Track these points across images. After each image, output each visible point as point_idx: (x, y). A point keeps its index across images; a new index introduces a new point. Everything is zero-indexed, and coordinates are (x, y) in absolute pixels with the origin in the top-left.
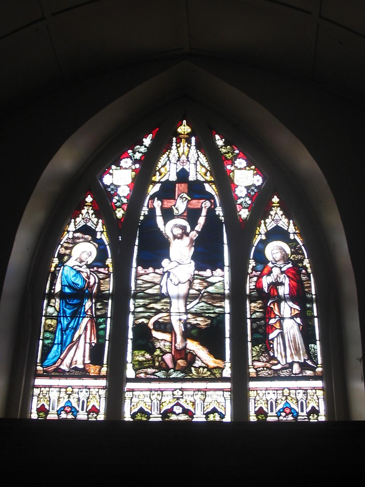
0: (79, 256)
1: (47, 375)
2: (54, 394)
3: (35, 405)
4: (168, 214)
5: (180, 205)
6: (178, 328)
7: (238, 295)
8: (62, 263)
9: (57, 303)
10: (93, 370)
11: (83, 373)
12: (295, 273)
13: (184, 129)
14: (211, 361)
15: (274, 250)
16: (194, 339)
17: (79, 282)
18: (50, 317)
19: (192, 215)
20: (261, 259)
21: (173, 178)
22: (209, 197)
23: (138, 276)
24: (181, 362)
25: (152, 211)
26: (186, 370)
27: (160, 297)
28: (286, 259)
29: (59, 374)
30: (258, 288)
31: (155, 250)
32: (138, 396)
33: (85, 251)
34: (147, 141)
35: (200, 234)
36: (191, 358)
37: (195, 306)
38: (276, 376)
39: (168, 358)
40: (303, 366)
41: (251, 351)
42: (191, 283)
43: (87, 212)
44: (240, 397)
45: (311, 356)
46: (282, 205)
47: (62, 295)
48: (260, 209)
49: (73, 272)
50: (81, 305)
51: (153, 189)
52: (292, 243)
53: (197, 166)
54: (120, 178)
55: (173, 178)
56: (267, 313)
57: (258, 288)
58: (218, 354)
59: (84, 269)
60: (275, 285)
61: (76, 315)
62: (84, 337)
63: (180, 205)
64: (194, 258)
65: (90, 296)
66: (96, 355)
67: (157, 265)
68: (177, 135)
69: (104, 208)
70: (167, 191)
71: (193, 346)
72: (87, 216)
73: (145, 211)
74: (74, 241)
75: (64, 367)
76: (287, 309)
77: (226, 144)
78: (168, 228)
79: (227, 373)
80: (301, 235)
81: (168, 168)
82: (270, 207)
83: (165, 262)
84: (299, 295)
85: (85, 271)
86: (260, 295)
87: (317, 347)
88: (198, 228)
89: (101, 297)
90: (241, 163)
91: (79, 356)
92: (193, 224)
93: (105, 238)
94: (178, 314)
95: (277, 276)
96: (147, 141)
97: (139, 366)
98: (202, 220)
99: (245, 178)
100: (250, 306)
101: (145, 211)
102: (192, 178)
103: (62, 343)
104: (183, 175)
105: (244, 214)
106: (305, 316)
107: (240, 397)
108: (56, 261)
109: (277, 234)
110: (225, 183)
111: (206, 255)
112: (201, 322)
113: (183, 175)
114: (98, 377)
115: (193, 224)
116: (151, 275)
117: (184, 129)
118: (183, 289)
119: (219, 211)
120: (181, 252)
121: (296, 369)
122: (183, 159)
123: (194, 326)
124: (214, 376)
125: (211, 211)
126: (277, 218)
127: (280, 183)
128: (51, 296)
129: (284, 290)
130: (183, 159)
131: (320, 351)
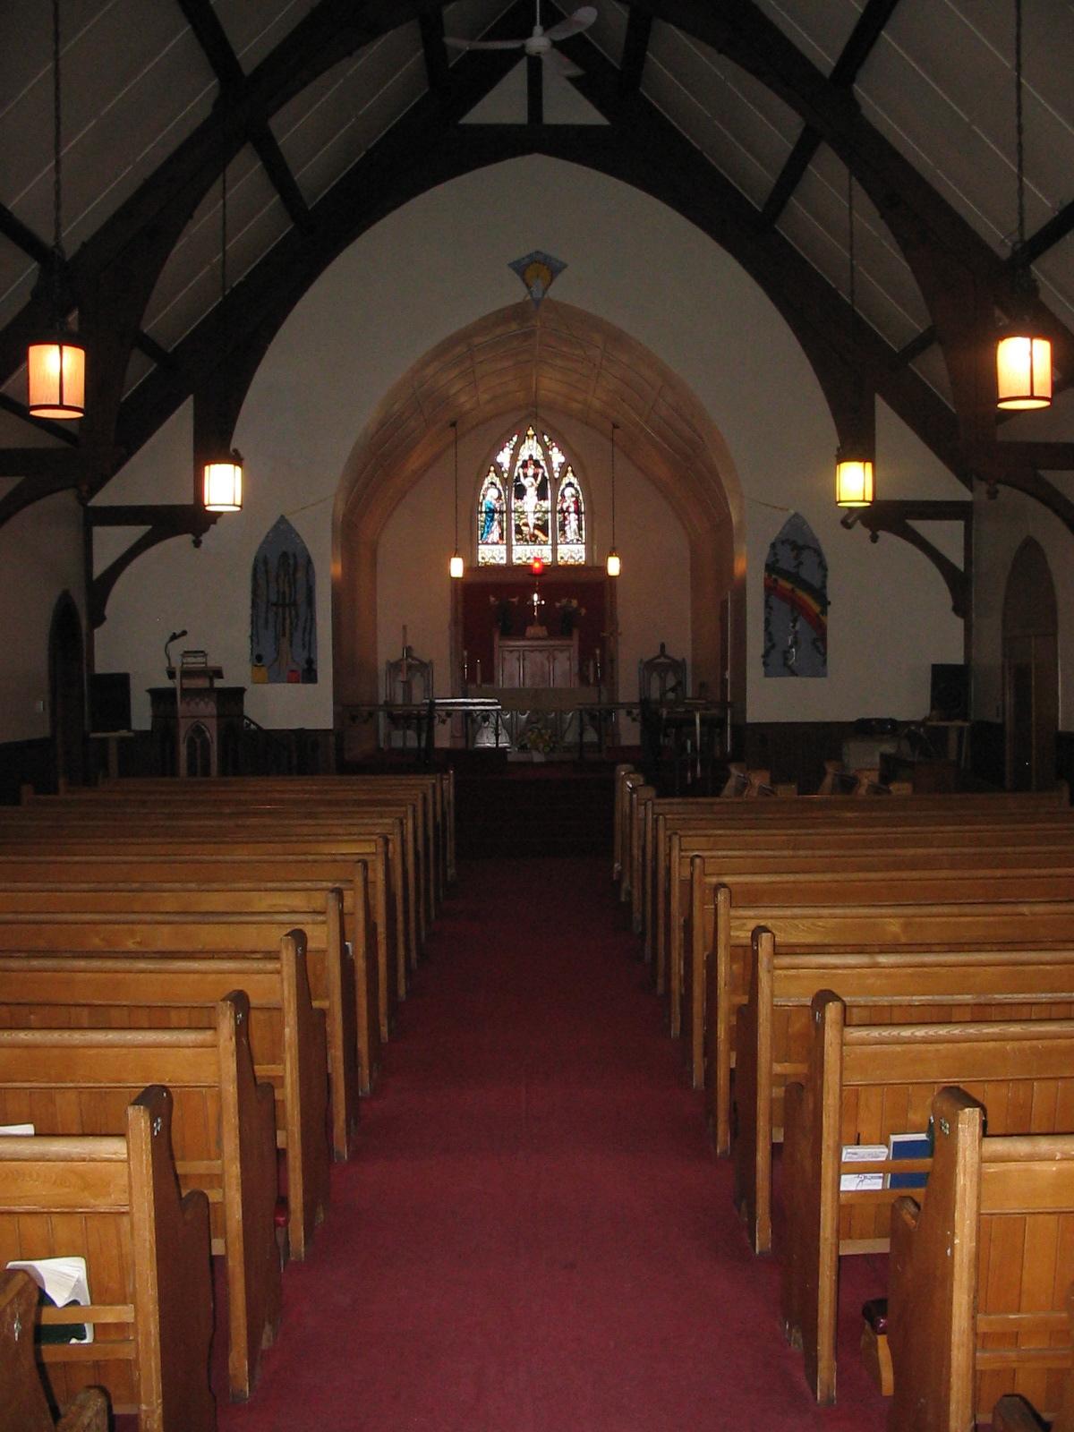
0: (490, 496)
1: (483, 544)
2: (487, 552)
3: (480, 556)
4: (526, 476)
5: (530, 471)
6: (531, 525)
7: (554, 511)
8: (484, 498)
9: (484, 515)
10: (500, 542)
11: (497, 543)
12: (577, 502)
13: (531, 432)
14: (543, 538)
15: (569, 492)
16: (538, 529)
17: (492, 507)
18: (482, 521)
19: (535, 476)
20: (563, 496)
21: (527, 458)
22: (542, 467)
23: (515, 503)
24: (533, 539)
25: (519, 474)
26: (535, 541)
27: (523, 513)
28: (573, 496)
29: (487, 543)
30: (562, 508)
31: (521, 492)
32: (917, 1205)
33: (493, 493)
34: (515, 439)
35: (539, 485)
36: (537, 537)
37: (539, 515)
38: (567, 543)
39: (528, 537)
40: (578, 540)
41: (559, 534)
42: (536, 507)
43: (492, 475)
44: (554, 551)
45: (581, 536)
46: (572, 471)
47: (486, 512)
48: (564, 474)
49: (520, 558)
50: (493, 516)
51: (519, 463)
52: (576, 489)
53: (537, 453)
54: (504, 457)
55: (527, 458)
56: (565, 519)
57: (562, 508)
58: (547, 535)
59: (661, 814)
60: (568, 507)
61: (492, 520)
62: (496, 530)
63: (530, 471)
64: (537, 495)
65: (497, 512)
66: (501, 536)
67: (522, 499)
68: (528, 435)
69: (498, 473)
70: (525, 465)
71: (537, 532)
72: (492, 477)
73: (516, 474)
74: (488, 488)
75: (489, 541)
76: (573, 517)
77: (550, 440)
78: (526, 482)
79: (550, 542)
80: (579, 485)
81: (524, 454)
82: (567, 472)
83: (525, 497)
84: (578, 512)
85: (494, 502)
86: (562, 511)
87: (583, 533)
88: (538, 482)
89: (501, 512)
90: (556, 450)
91: (495, 536)
92: (536, 480)
93: (501, 488)
94: (531, 520)
95: (569, 503)
96: (515, 439)
97: (518, 540)
98: (539, 478)
99: (557, 457)
100: (558, 515)
101: (516, 474)
102: (534, 458)
103: (488, 532)
104: (531, 457)
105: (557, 475)
106: (579, 520)
107: (554, 551)
108: (481, 497)
109: (570, 485)
110: (548, 459)
111: (542, 494)
112: (540, 523)
113: (531, 457)
114: (503, 544)
115: (536, 480)
116: (519, 503)
117: (531, 432)
118: (533, 509)
119: (546, 475)
120: (531, 493)
121: (575, 541)
122: (531, 449)
123: (538, 525)
124: (545, 543)
125: (543, 474)
126: (570, 478)
127: (575, 462)
128: (481, 512)
129: (572, 509)
130: (531, 449)
131: (455, 622)
